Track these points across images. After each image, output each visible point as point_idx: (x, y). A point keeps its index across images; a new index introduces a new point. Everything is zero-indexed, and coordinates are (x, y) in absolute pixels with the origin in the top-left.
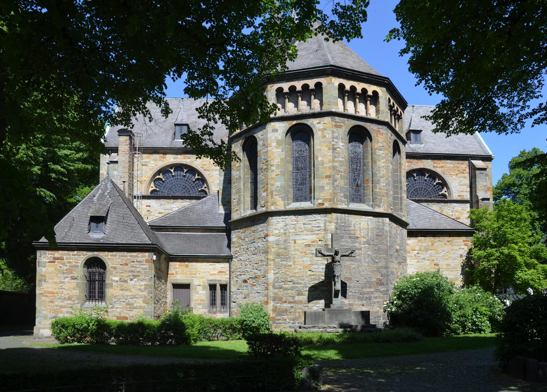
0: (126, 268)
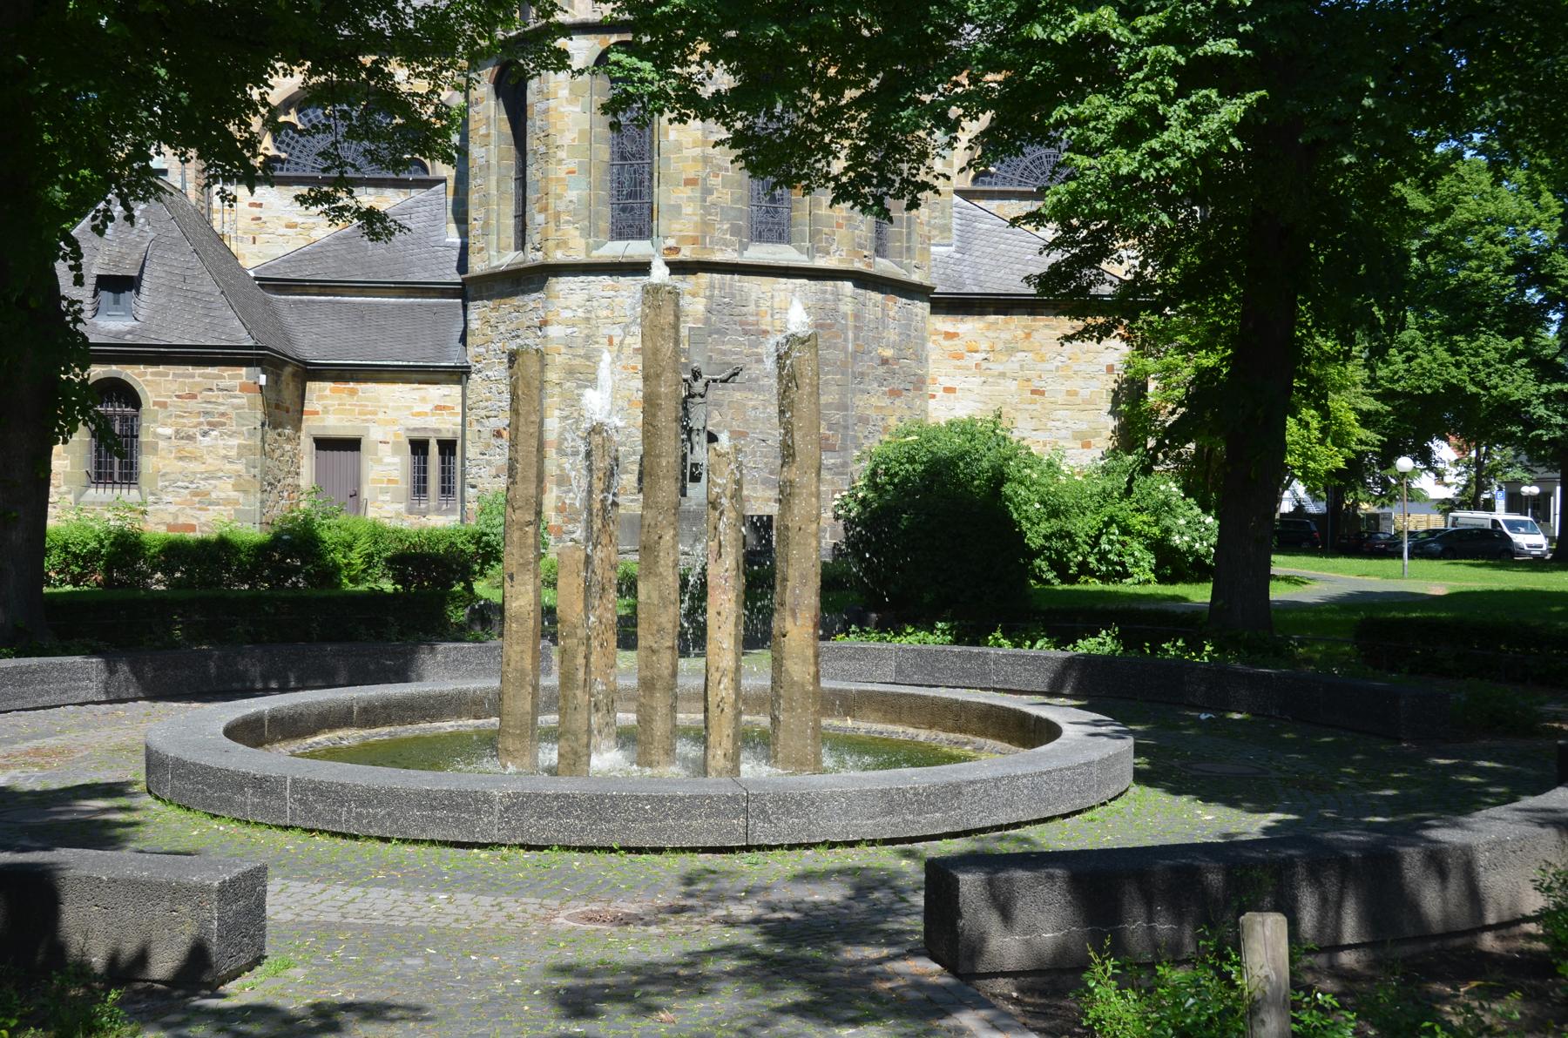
0: (192, 405)
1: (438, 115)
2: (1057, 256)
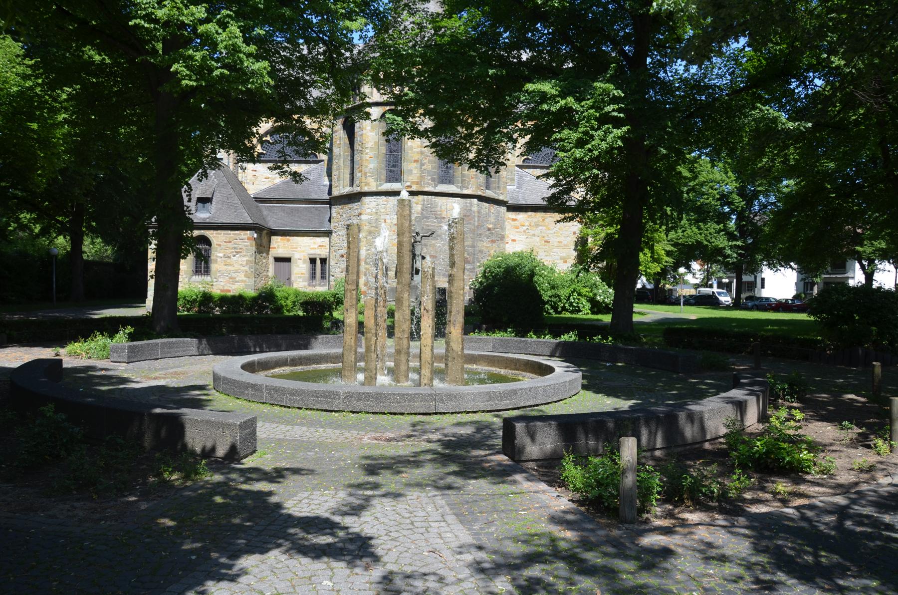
0: (230, 245)
1: (321, 137)
2: (554, 190)
